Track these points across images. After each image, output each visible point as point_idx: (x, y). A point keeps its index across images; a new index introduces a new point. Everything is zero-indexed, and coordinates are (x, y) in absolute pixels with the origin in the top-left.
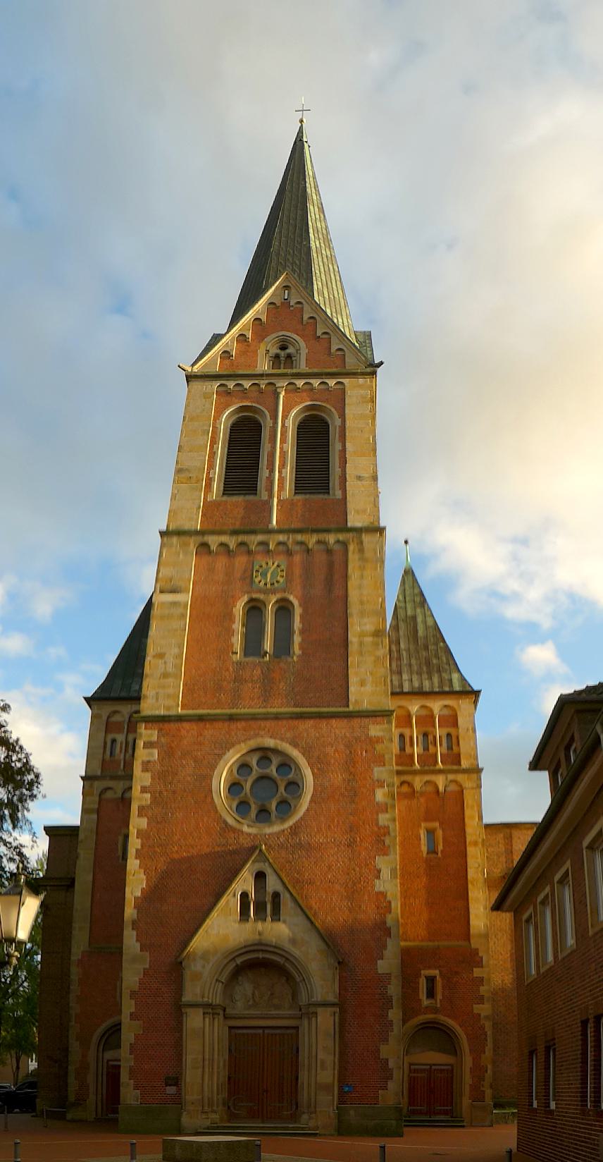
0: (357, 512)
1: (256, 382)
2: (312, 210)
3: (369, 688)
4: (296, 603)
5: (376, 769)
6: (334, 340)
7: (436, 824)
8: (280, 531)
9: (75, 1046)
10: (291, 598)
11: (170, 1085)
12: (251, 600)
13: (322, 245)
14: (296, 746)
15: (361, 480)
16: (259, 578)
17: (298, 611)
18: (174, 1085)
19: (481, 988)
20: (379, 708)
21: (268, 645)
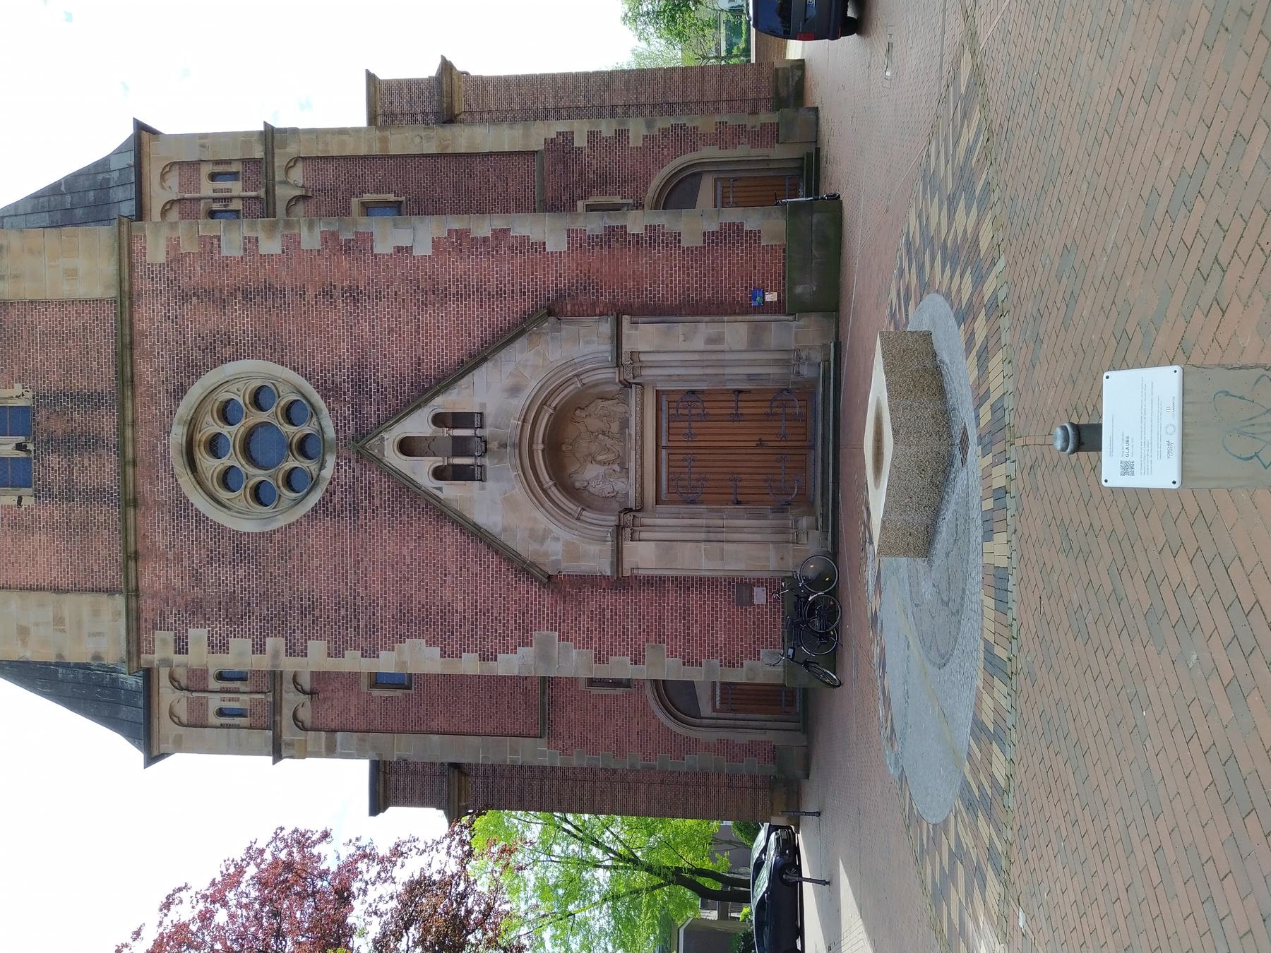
7: (355, 201)
9: (691, 761)
11: (752, 597)
18: (752, 591)
19: (604, 134)
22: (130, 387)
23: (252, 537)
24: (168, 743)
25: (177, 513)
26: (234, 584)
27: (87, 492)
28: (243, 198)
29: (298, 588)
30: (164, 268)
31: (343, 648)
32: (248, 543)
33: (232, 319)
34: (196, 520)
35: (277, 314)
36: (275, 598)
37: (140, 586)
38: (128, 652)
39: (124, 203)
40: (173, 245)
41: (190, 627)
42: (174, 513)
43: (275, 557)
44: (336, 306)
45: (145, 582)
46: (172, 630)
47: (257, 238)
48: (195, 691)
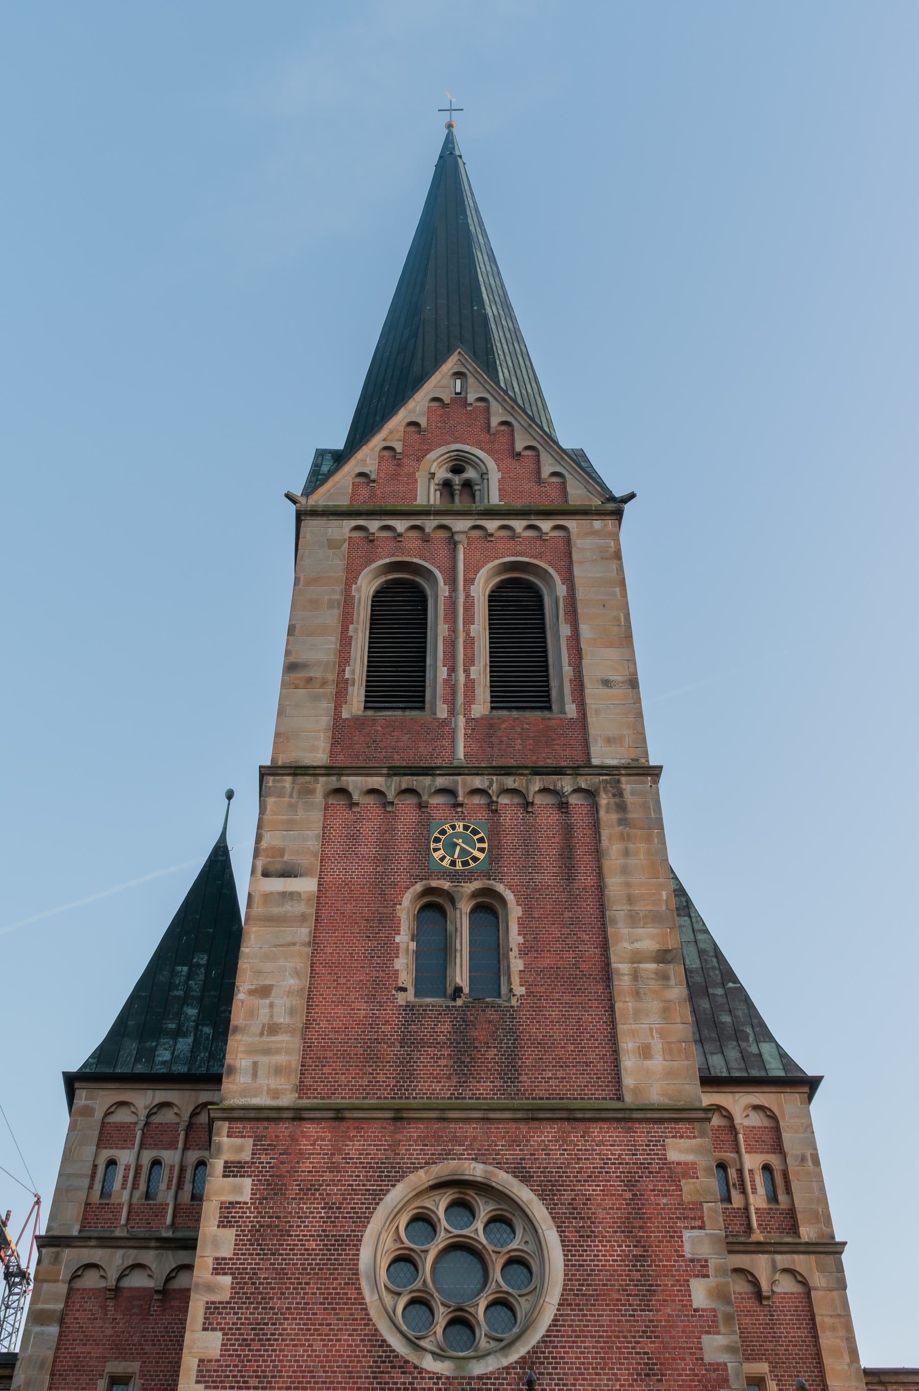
0: (609, 741)
1: (418, 523)
2: (481, 258)
3: (657, 1063)
4: (510, 896)
6: (545, 459)
7: (763, 1368)
8: (477, 771)
10: (500, 888)
12: (429, 891)
13: (501, 312)
14: (525, 1178)
16: (441, 853)
17: (515, 911)
21: (461, 976)
22: (525, 1116)
23: (353, 1260)
24: (86, 1099)
25: (385, 1168)
26: (299, 1235)
27: (409, 1062)
28: (746, 1208)
29: (287, 1319)
30: (661, 1159)
31: (207, 1382)
32: (346, 1255)
33: (610, 1241)
34: (375, 1190)
35: (620, 1300)
36: (279, 1289)
37: (303, 1122)
38: (232, 1109)
40: (688, 1170)
41: (253, 1180)
42: (385, 1163)
43: (329, 1288)
44: (636, 1380)
45: (311, 1129)
46: (253, 1158)
47: (708, 1276)
48: (143, 1133)
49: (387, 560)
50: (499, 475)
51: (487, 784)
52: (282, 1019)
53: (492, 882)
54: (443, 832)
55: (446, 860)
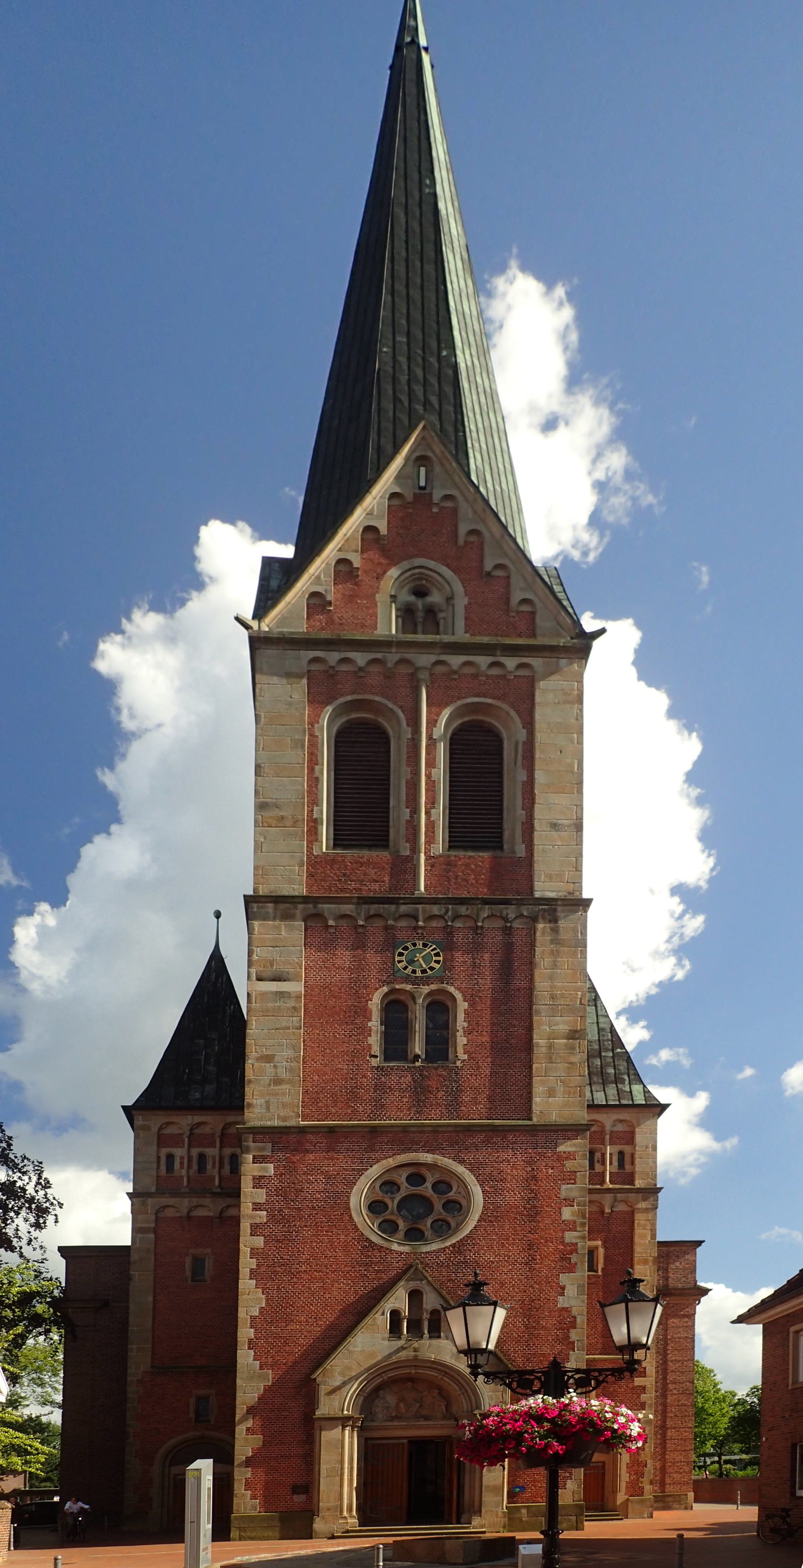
1: (379, 656)
4: (458, 996)
5: (564, 1187)
6: (516, 582)
8: (434, 901)
10: (452, 989)
11: (299, 1493)
12: (392, 991)
15: (558, 831)
16: (404, 964)
17: (462, 1006)
18: (303, 1493)
20: (571, 1122)
21: (418, 1047)
39: (604, 1095)
49: (349, 698)
50: (466, 601)
51: (443, 911)
52: (283, 1074)
53: (445, 985)
54: (406, 948)
55: (408, 969)
